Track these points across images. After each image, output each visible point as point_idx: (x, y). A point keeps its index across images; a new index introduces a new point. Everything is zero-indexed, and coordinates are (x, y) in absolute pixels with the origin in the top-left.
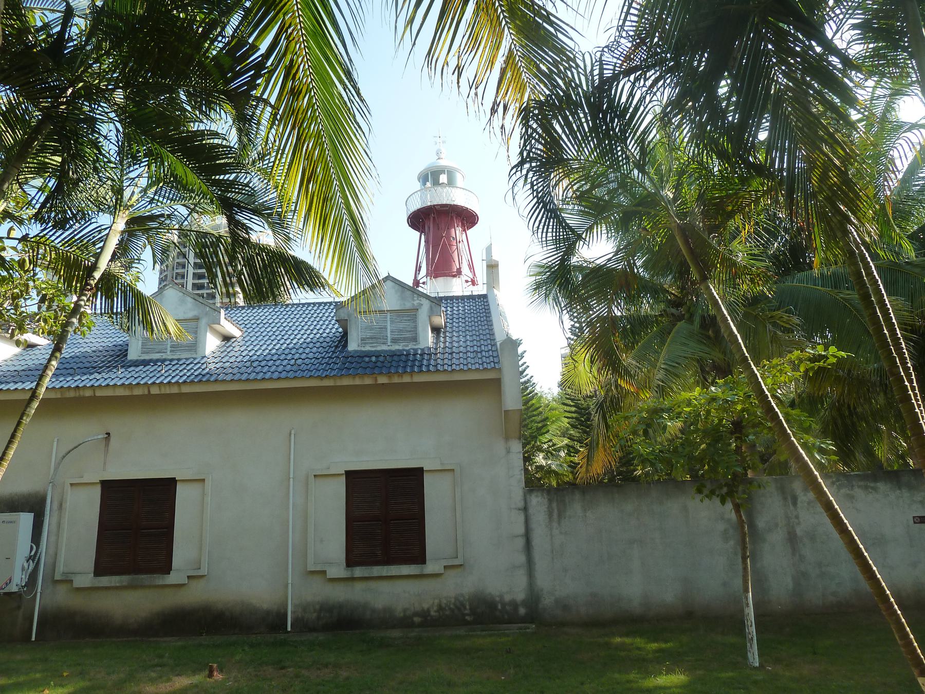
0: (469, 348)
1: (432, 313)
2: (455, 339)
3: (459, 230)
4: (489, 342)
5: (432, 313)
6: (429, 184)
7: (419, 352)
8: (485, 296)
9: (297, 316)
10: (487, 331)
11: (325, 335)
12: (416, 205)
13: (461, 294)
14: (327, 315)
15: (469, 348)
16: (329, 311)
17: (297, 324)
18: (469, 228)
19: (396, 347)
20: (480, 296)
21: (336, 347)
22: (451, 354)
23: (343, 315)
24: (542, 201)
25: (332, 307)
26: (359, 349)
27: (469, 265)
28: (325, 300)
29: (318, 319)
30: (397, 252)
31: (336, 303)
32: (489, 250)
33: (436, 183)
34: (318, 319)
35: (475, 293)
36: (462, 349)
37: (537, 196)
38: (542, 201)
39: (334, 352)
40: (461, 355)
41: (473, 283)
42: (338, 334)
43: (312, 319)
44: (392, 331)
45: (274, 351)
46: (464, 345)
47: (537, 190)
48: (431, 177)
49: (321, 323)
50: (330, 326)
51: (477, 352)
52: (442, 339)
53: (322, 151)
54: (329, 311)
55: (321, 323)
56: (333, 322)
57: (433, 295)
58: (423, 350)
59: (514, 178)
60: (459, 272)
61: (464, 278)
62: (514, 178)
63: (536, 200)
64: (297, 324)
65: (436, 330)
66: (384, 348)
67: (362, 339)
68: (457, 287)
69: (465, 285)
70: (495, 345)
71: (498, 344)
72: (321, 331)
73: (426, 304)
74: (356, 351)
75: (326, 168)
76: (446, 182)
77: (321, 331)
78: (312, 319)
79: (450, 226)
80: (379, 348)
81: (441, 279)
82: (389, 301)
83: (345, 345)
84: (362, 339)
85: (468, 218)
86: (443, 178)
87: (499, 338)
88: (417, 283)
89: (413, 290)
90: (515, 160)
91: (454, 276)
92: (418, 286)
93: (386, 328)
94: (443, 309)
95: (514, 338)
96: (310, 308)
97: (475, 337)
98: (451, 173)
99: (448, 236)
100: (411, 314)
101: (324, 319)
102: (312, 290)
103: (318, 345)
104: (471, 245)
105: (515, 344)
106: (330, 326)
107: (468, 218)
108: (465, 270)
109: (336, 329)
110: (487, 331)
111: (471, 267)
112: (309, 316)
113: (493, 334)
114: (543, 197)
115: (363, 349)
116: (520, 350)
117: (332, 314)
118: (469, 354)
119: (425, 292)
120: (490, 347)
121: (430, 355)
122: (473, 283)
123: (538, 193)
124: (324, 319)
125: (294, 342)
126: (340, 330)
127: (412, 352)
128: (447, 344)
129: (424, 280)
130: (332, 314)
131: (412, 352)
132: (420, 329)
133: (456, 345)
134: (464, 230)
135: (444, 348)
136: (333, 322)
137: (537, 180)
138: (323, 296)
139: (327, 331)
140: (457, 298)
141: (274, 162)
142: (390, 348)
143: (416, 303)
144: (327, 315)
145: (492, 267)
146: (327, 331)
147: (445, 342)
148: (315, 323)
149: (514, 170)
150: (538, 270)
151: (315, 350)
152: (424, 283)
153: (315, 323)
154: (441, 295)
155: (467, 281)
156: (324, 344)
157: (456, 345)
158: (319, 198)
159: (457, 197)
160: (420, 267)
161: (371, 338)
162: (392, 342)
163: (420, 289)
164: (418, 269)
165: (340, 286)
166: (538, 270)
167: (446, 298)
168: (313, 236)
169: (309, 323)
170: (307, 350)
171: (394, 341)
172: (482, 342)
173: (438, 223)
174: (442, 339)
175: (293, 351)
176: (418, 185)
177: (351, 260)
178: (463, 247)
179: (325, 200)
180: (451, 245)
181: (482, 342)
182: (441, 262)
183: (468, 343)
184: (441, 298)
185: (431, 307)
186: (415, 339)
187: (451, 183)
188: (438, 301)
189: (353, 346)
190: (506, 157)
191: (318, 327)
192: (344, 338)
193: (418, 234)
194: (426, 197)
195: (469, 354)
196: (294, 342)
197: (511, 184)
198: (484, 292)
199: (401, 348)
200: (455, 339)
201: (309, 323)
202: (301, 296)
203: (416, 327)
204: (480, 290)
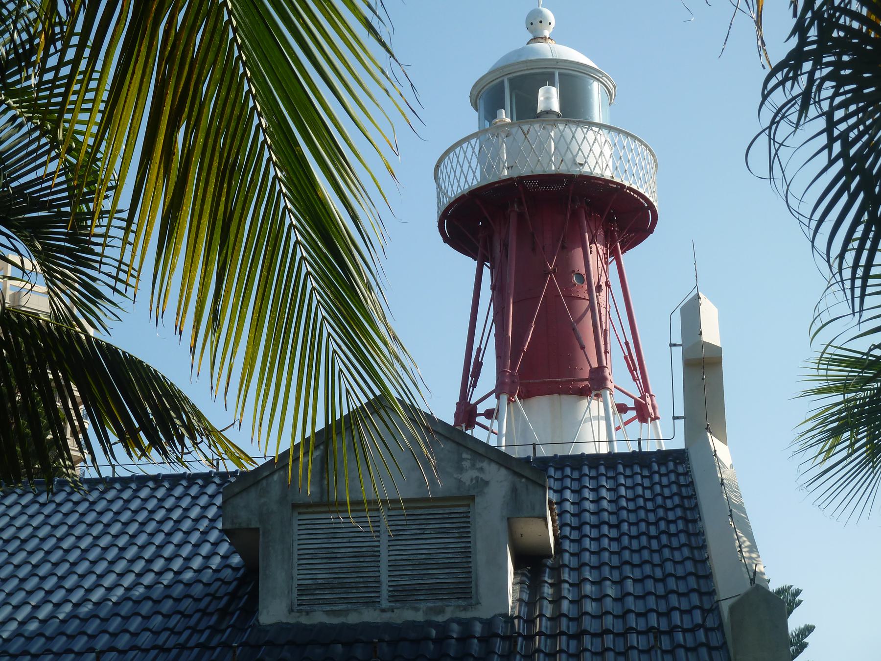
0: (632, 620)
1: (518, 508)
2: (588, 589)
3: (596, 252)
4: (695, 599)
5: (518, 508)
6: (504, 116)
7: (478, 628)
8: (678, 457)
9: (107, 518)
10: (690, 566)
11: (188, 576)
12: (467, 176)
13: (604, 449)
14: (195, 512)
15: (632, 620)
16: (204, 500)
17: (105, 541)
18: (629, 245)
19: (407, 615)
20: (663, 456)
21: (224, 613)
22: (578, 636)
23: (246, 511)
24: (860, 170)
25: (211, 489)
26: (292, 620)
27: (628, 358)
28: (152, 471)
29: (168, 527)
30: (432, 315)
31: (224, 476)
32: (690, 313)
33: (527, 110)
34: (168, 527)
35: (649, 447)
36: (609, 621)
37: (843, 154)
38: (860, 170)
39: (215, 630)
40: (609, 640)
41: (643, 413)
42: (227, 573)
43: (151, 527)
44: (394, 566)
45: (33, 626)
46: (618, 610)
47: (844, 136)
48: (510, 92)
49: (177, 538)
50: (205, 549)
51: (657, 632)
52: (548, 591)
53: (217, 32)
54: (204, 500)
55: (177, 538)
56: (214, 536)
57: (517, 453)
58: (488, 623)
59: (778, 98)
60: (597, 383)
61: (614, 398)
62: (778, 98)
63: (839, 165)
64: (105, 541)
65: (530, 562)
66: (370, 616)
67: (303, 590)
68: (595, 429)
69: (616, 419)
70: (715, 609)
71: (725, 607)
72: (177, 565)
73: (499, 481)
74: (281, 627)
75: (229, 80)
76: (556, 107)
77: (177, 565)
78: (151, 527)
79: (570, 239)
80: (353, 619)
81: (541, 403)
82: (383, 476)
83: (252, 607)
84: (303, 590)
85: (624, 217)
86: (549, 98)
87: (728, 589)
88: (467, 413)
89: (454, 438)
90: (781, 46)
91: (584, 393)
92: (471, 424)
93: (374, 555)
94: (549, 495)
95: (773, 587)
96: (144, 493)
97: (650, 585)
98: (572, 81)
99: (565, 271)
100: (452, 512)
101: (186, 525)
102: (155, 442)
103: (168, 605)
104: (638, 297)
105: (787, 601)
106: (205, 549)
107: (624, 217)
108: (618, 374)
109: (220, 555)
110: (690, 566)
111: (636, 365)
112: (142, 516)
113: (709, 577)
114: (861, 157)
115: (304, 620)
116: (795, 623)
117: (212, 512)
118: (633, 639)
119: (493, 442)
120: (698, 616)
121: (510, 639)
122: (643, 413)
123: (847, 145)
124: (186, 525)
125: (96, 596)
126: (236, 560)
127: (455, 630)
128: (565, 605)
129: (491, 403)
130: (212, 512)
131: (455, 630)
132: (480, 559)
133: (589, 606)
134: (614, 253)
135: (556, 618)
136: (214, 536)
137: (844, 105)
138: (198, 460)
139: (197, 563)
140: (595, 460)
141: (75, 62)
142: (386, 617)
143: (468, 477)
144: (195, 512)
145: (703, 367)
146: (197, 563)
147: (557, 601)
148: (159, 539)
149: (780, 76)
150: (838, 372)
151: (157, 621)
152: (489, 414)
153: (159, 539)
154: (543, 452)
155: (622, 409)
156: (187, 604)
157: (589, 606)
158: (205, 171)
159: (597, 155)
160: (479, 365)
161: (330, 586)
162: (393, 598)
163: (478, 433)
164: (472, 371)
165: (247, 419)
166: (838, 372)
167: (561, 462)
168: (206, 275)
169: (141, 539)
170: (135, 624)
171: (403, 595)
172: (674, 600)
173: (539, 230)
174: (548, 591)
175: (93, 627)
176: (470, 120)
177: (313, 346)
178: (610, 303)
179: (228, 172)
180: (572, 298)
181: (674, 600)
182: (544, 353)
183: (630, 602)
184: (544, 463)
185: (514, 490)
186: (465, 590)
187: (574, 110)
188: (534, 472)
189: (273, 611)
190: (754, 44)
191: (168, 551)
192: (246, 585)
193: (472, 264)
194: (497, 153)
195: (633, 639)
196: (96, 596)
197: (768, 115)
198: (679, 443)
199: (419, 617)
200: (588, 589)
201: (141, 539)
202: (104, 458)
203: (467, 553)
204: (665, 434)
